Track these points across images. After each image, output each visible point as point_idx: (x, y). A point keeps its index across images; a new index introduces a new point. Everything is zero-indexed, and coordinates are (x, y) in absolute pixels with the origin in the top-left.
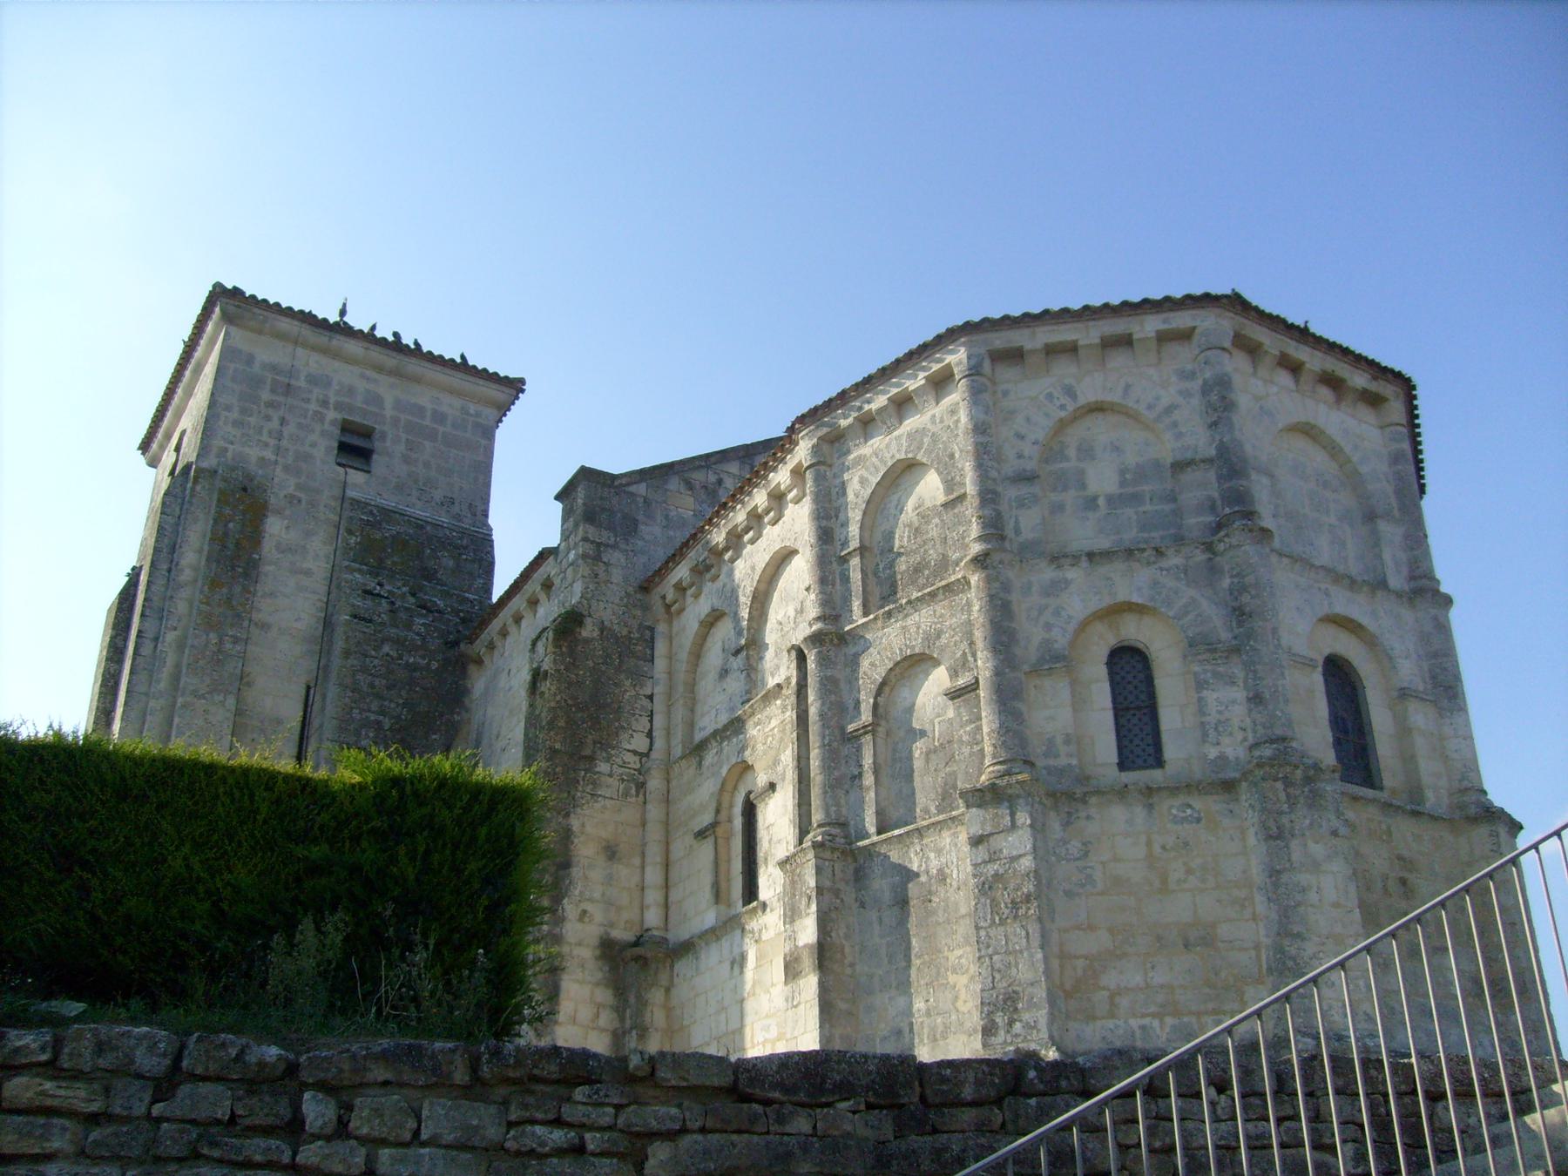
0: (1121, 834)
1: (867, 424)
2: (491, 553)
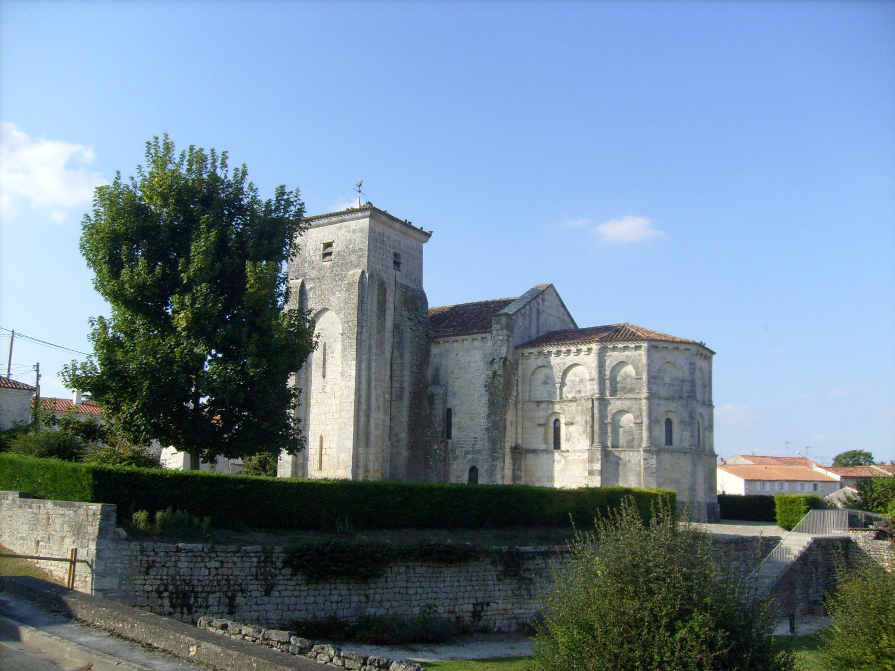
0: (666, 457)
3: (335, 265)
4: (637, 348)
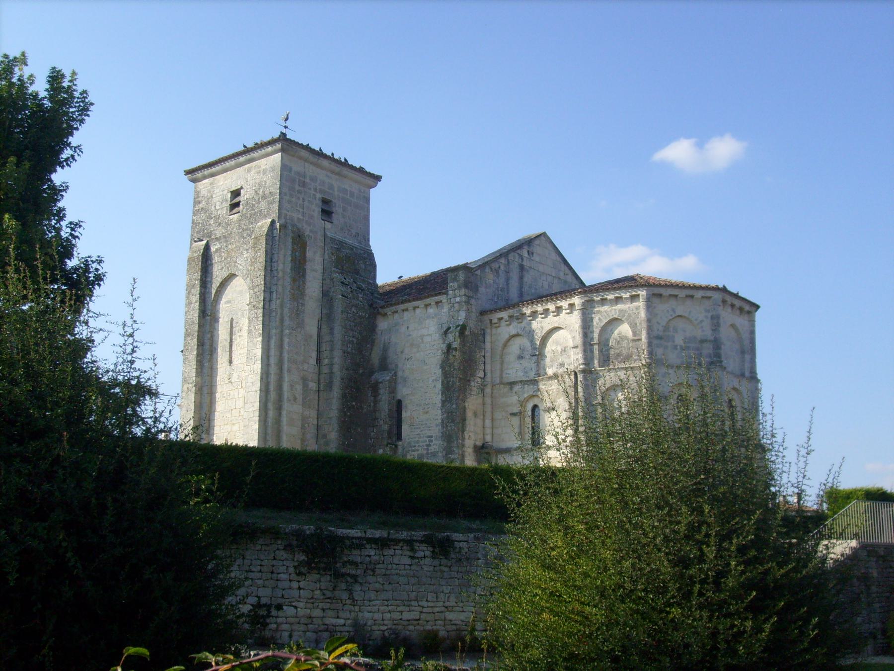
1: (603, 301)
2: (374, 260)
3: (244, 216)
4: (634, 298)
